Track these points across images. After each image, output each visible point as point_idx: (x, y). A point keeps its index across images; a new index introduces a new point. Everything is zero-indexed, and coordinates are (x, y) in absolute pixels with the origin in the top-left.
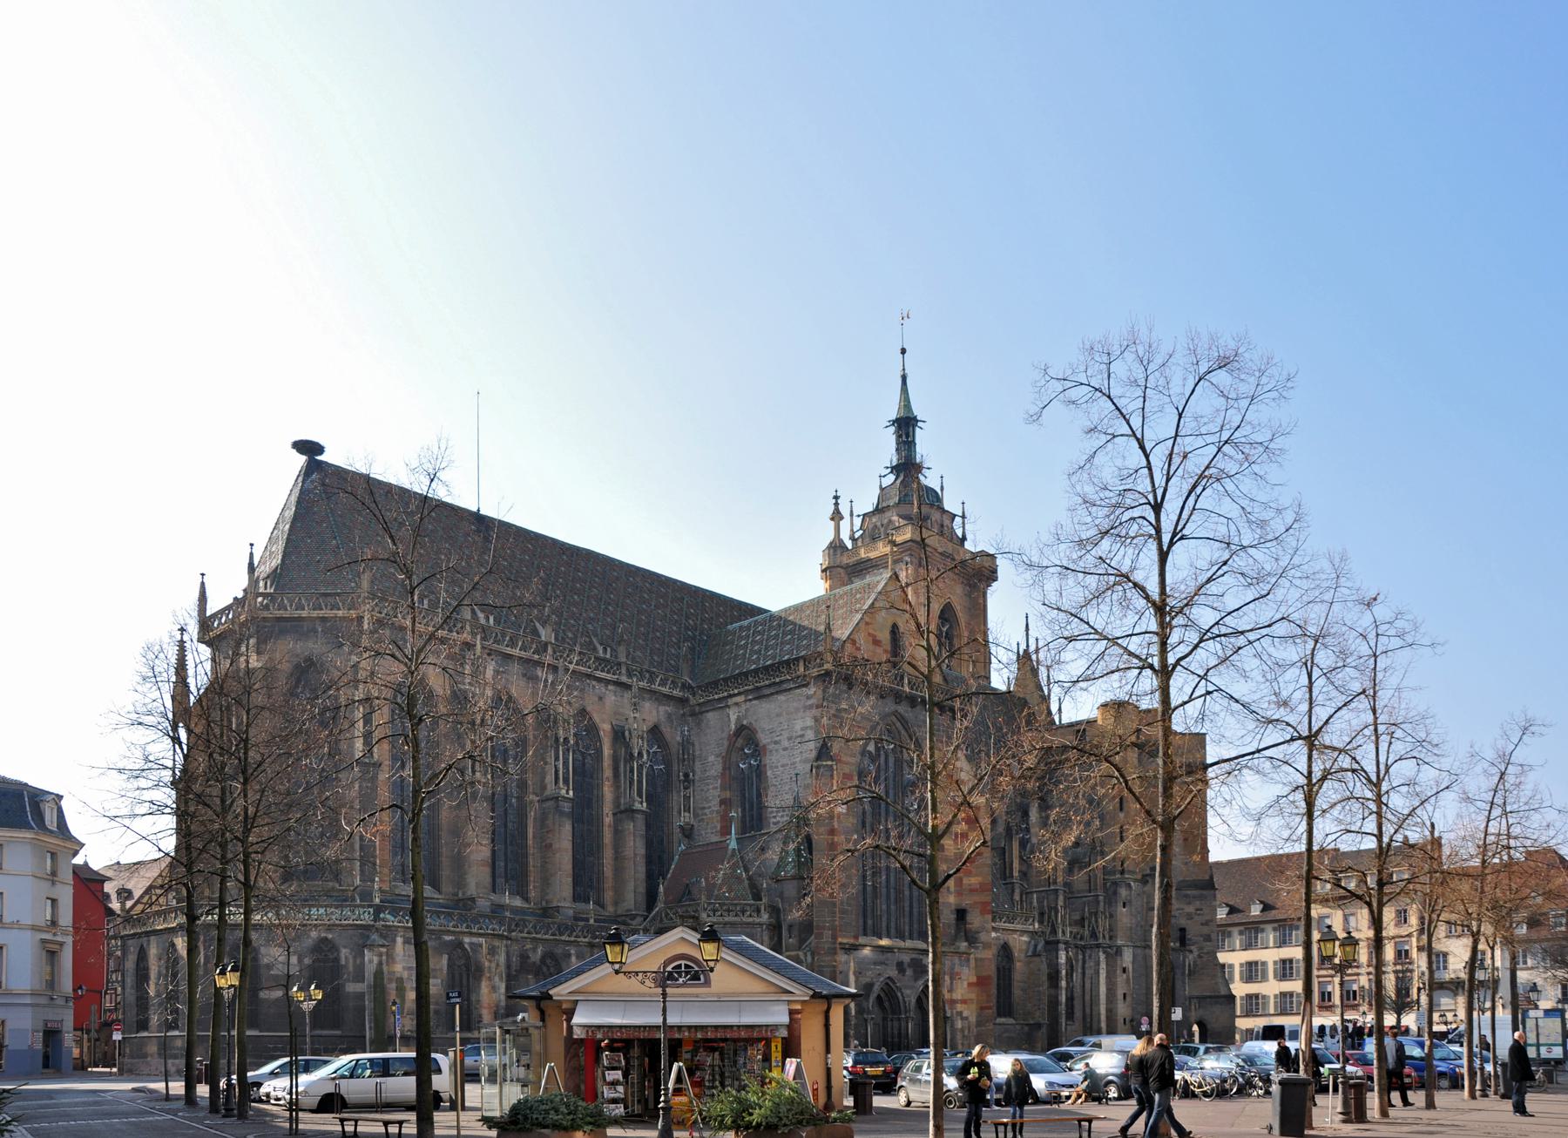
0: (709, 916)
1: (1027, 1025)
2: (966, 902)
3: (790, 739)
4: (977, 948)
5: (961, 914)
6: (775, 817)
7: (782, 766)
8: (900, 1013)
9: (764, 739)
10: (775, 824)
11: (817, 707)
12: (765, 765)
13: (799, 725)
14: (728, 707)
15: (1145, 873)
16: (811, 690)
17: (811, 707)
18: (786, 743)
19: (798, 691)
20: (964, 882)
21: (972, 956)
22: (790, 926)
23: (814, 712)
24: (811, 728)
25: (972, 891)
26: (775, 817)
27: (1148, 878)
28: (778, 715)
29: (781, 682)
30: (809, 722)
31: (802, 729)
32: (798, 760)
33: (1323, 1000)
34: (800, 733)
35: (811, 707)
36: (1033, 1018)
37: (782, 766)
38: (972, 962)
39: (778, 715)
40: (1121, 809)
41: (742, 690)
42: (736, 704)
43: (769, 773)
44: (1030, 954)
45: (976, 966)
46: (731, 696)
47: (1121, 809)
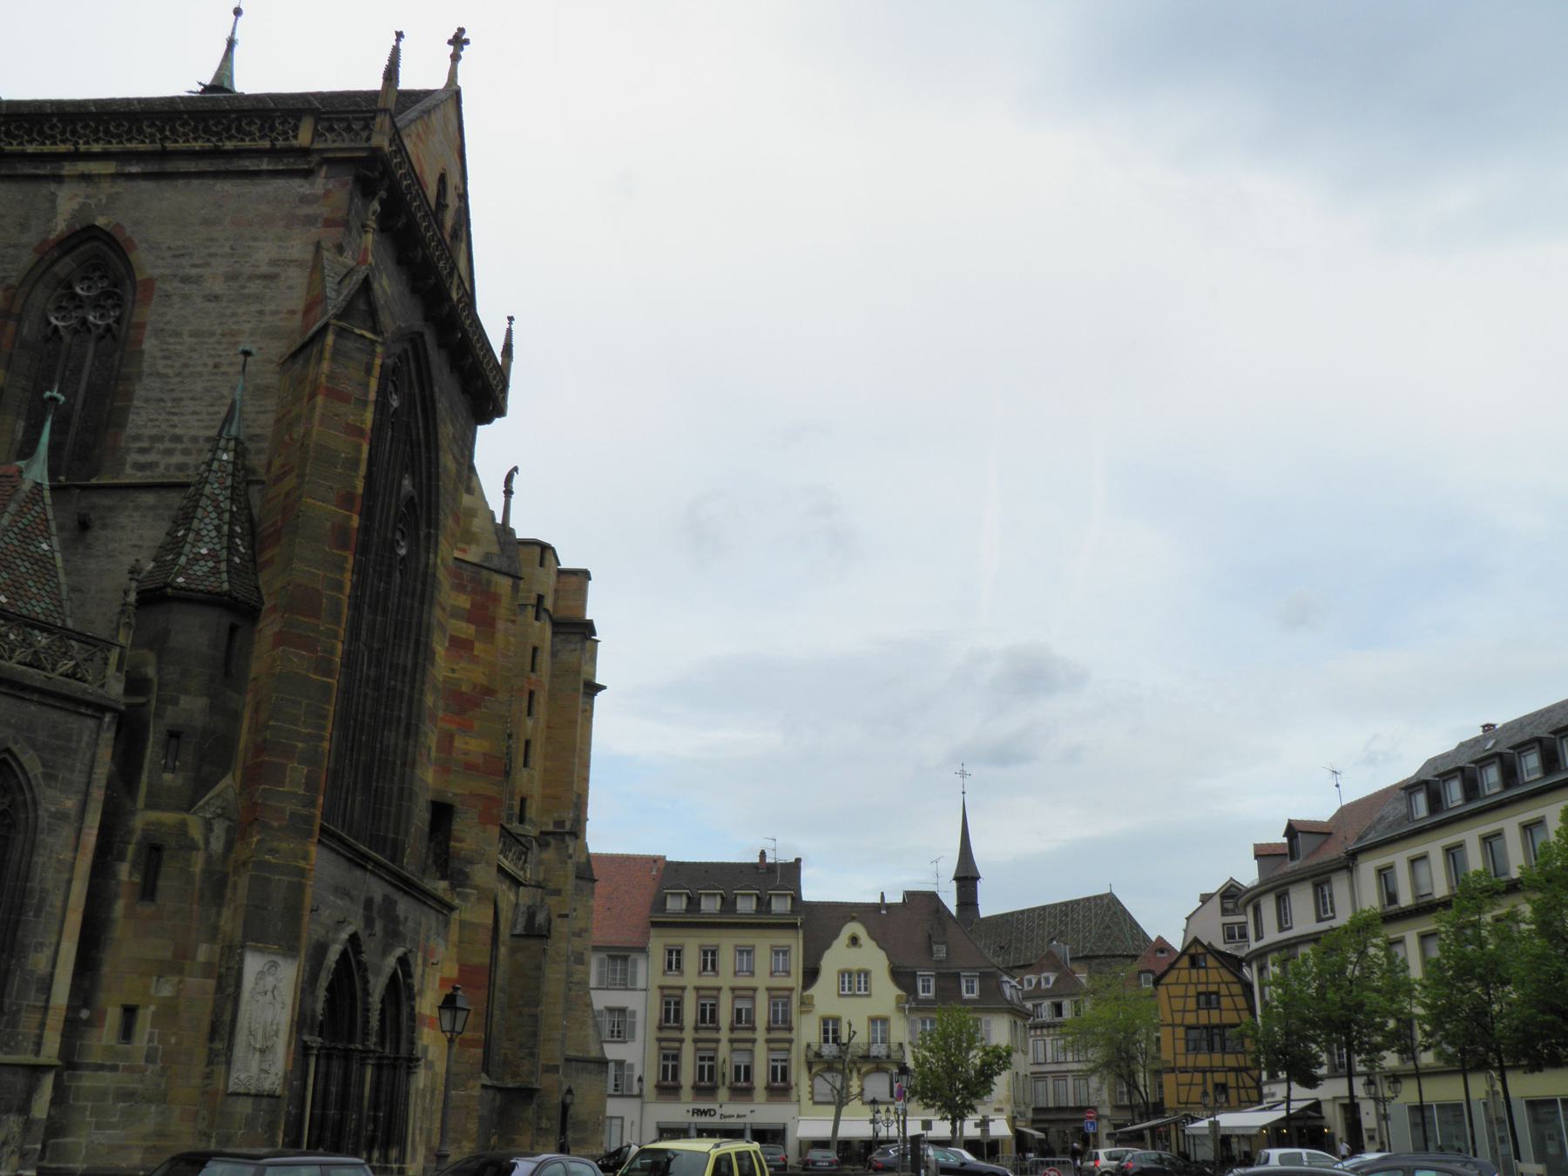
0: (141, 537)
1: (499, 1089)
2: (456, 789)
3: (231, 277)
4: (465, 897)
5: (442, 813)
6: (142, 451)
7: (193, 334)
8: (351, 1040)
9: (147, 263)
10: (140, 467)
11: (329, 223)
12: (142, 326)
13: (263, 254)
14: (59, 179)
15: (545, 829)
16: (319, 184)
17: (309, 221)
18: (218, 287)
19: (280, 183)
20: (456, 744)
21: (455, 915)
22: (174, 735)
23: (316, 232)
24: (300, 264)
25: (469, 767)
26: (142, 451)
27: (551, 839)
28: (206, 222)
29: (238, 153)
30: (298, 247)
31: (273, 263)
32: (247, 327)
33: (738, 1079)
34: (264, 269)
35: (309, 221)
36: (515, 1075)
37: (193, 334)
38: (454, 929)
39: (206, 222)
40: (529, 714)
41: (115, 147)
42: (86, 178)
43: (149, 345)
44: (519, 930)
45: (461, 941)
46: (77, 156)
47: (529, 714)
